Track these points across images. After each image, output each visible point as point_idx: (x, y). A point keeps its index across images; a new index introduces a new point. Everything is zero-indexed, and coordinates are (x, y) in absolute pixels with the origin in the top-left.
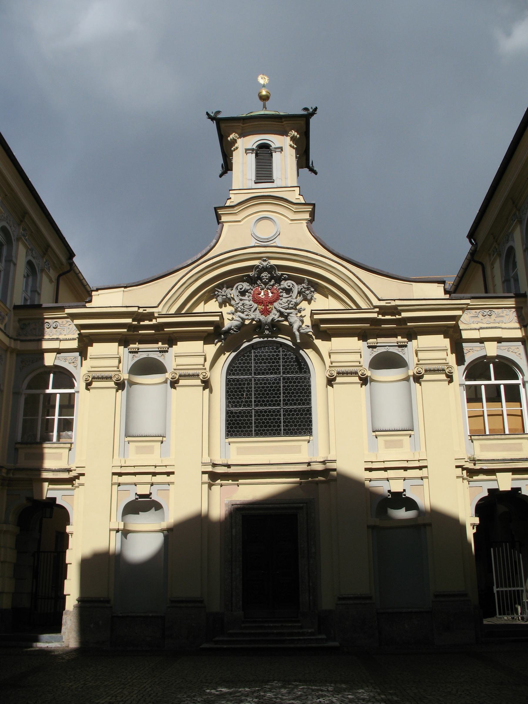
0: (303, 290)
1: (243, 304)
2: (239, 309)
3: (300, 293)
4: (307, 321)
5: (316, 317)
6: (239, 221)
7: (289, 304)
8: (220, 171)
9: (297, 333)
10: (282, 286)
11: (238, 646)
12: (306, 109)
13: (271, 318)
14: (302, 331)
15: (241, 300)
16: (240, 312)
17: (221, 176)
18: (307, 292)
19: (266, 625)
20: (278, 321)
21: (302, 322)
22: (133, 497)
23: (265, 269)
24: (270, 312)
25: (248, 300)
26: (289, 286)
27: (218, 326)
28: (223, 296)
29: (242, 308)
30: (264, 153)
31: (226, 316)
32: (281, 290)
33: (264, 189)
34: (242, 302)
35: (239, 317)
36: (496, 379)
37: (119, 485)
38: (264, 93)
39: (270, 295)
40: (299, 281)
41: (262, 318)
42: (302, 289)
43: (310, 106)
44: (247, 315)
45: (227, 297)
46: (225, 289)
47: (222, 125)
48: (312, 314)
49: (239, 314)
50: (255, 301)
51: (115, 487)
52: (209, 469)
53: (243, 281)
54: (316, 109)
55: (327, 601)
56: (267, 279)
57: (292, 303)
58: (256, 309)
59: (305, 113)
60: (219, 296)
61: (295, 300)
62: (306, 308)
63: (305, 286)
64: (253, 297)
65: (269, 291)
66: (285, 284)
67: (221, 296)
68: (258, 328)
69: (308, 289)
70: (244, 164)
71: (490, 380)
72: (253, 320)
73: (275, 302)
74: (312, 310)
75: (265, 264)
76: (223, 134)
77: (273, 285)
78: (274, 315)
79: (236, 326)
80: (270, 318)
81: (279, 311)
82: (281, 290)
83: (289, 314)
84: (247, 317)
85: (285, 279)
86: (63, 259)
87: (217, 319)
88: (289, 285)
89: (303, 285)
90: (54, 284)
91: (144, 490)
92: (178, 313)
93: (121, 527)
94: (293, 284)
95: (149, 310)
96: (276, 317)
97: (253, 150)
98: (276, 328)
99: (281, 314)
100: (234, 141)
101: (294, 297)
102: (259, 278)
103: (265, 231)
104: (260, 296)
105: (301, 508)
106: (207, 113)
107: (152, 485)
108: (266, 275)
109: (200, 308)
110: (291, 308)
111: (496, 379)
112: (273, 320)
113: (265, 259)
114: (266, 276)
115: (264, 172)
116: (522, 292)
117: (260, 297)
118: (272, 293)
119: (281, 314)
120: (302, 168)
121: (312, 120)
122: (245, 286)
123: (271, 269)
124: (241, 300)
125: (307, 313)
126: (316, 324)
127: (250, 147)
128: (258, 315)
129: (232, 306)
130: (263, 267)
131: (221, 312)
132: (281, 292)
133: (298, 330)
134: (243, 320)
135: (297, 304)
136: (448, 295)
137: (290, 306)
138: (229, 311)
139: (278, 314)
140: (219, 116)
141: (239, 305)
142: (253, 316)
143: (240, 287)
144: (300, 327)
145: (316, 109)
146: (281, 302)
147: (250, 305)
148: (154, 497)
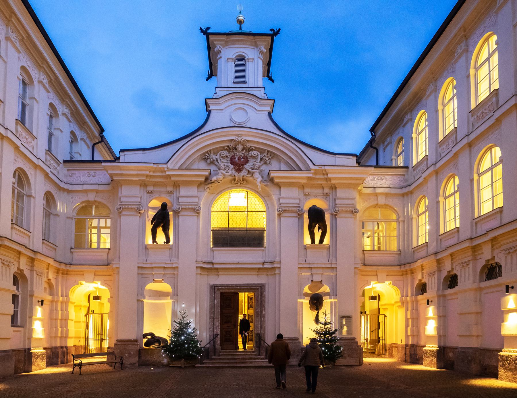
6: (222, 110)
8: (207, 76)
10: (250, 155)
11: (217, 365)
12: (272, 30)
17: (207, 80)
30: (241, 62)
38: (241, 18)
39: (242, 160)
43: (276, 29)
47: (211, 38)
54: (280, 29)
70: (226, 71)
76: (211, 46)
86: (97, 134)
90: (91, 149)
97: (233, 59)
100: (219, 52)
103: (239, 118)
106: (201, 28)
109: (195, 166)
115: (240, 76)
119: (249, 172)
121: (275, 38)
127: (230, 57)
136: (376, 192)
139: (247, 172)
140: (209, 31)
143: (223, 154)
145: (280, 29)
146: (249, 164)
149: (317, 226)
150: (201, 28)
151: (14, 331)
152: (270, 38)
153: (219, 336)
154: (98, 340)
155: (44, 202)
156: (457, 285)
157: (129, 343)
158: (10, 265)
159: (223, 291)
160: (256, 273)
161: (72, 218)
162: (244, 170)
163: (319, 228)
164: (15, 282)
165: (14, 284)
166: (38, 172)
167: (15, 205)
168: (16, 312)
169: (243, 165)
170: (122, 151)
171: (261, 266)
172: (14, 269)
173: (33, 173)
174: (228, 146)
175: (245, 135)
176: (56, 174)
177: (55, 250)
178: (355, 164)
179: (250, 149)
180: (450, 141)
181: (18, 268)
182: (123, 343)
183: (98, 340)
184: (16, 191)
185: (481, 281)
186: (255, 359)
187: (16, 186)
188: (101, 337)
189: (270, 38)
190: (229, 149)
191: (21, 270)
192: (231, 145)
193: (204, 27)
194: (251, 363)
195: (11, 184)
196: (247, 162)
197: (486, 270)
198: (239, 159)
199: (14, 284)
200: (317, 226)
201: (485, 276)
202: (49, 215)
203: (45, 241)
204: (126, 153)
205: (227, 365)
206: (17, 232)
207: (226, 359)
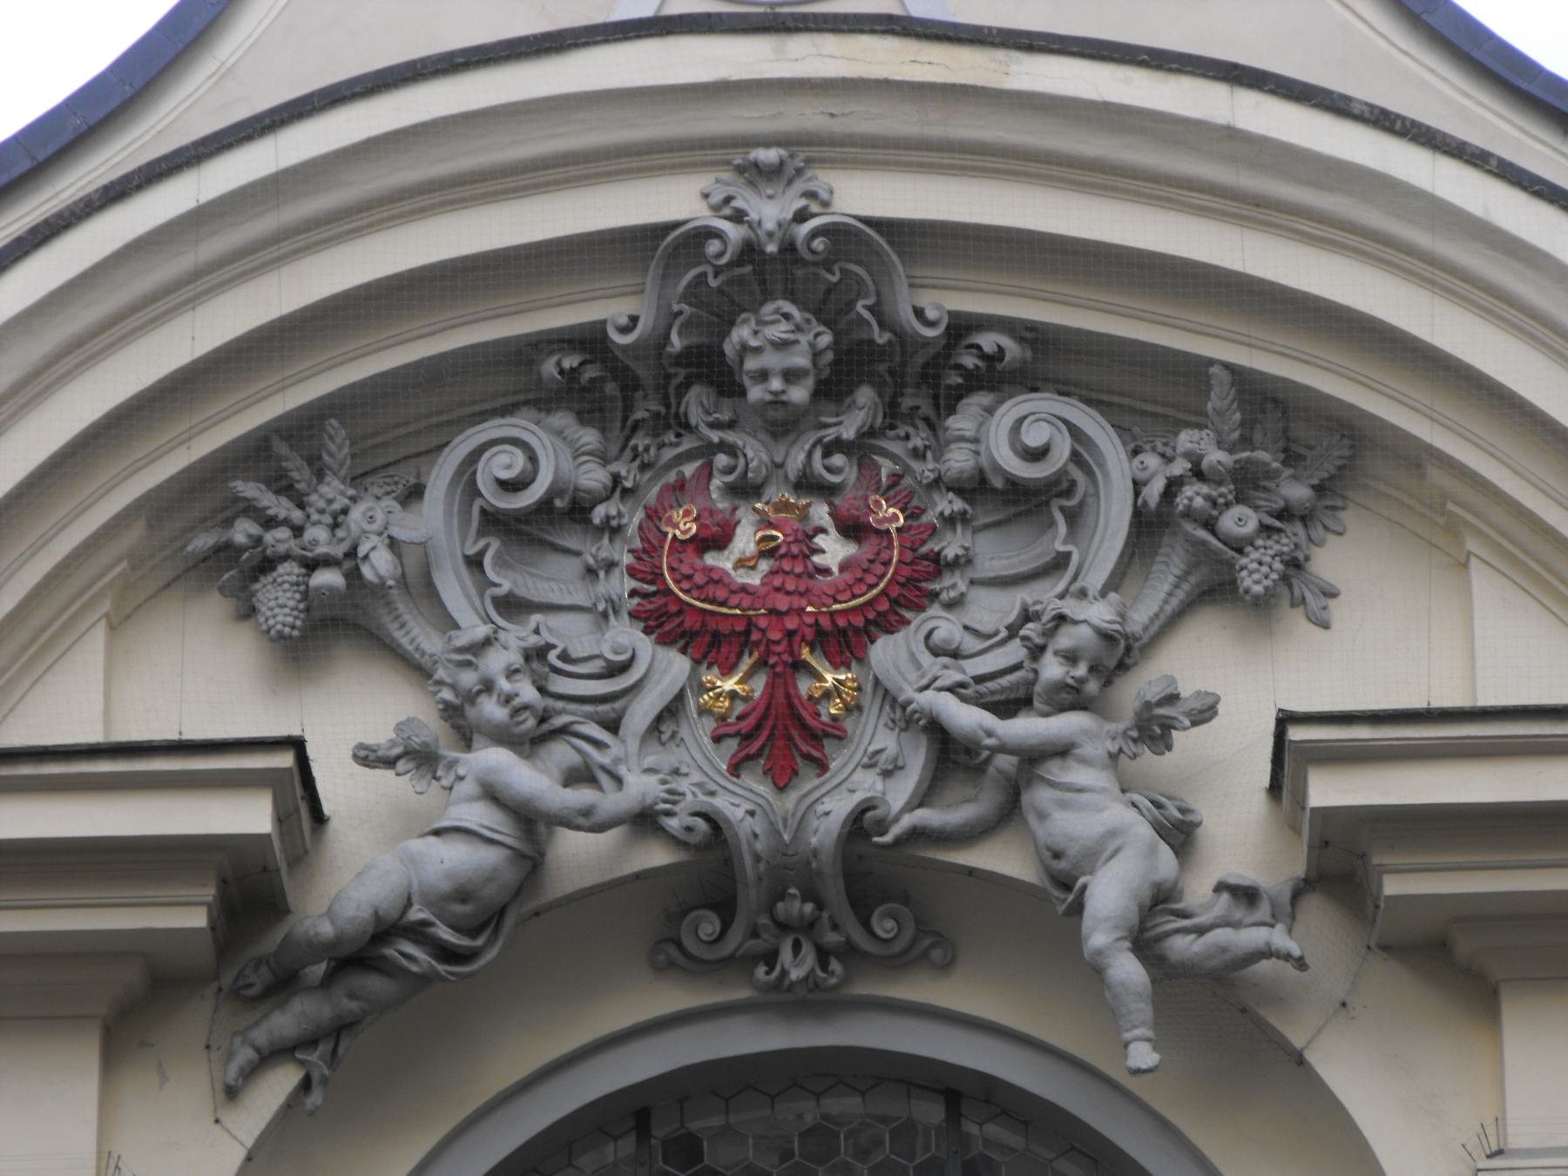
0: (1193, 495)
1: (536, 654)
2: (492, 710)
3: (1149, 526)
4: (1241, 836)
5: (1329, 790)
7: (1037, 652)
9: (1127, 970)
10: (959, 460)
13: (839, 807)
14: (1182, 946)
15: (512, 606)
16: (503, 737)
18: (1239, 520)
20: (918, 834)
21: (1180, 834)
23: (767, 270)
24: (836, 733)
25: (585, 615)
26: (1037, 455)
27: (250, 887)
28: (311, 565)
29: (527, 692)
31: (337, 781)
32: (948, 504)
34: (518, 635)
35: (492, 794)
40: (1142, 422)
41: (743, 803)
42: (1172, 487)
44: (580, 776)
45: (354, 576)
46: (333, 490)
48: (1287, 763)
49: (494, 759)
50: (663, 620)
53: (544, 401)
56: (791, 376)
57: (1066, 639)
58: (672, 710)
60: (267, 565)
61: (1100, 613)
62: (1239, 686)
63: (1215, 457)
64: (644, 570)
65: (820, 513)
66: (1005, 433)
67: (289, 571)
68: (705, 901)
69: (1246, 484)
72: (645, 821)
73: (885, 620)
74: (1286, 720)
75: (770, 211)
77: (860, 449)
78: (874, 777)
79: (462, 894)
80: (830, 803)
81: (909, 720)
82: (948, 504)
83: (1034, 758)
84: (581, 796)
85: (996, 378)
87: (250, 816)
88: (1034, 436)
89: (1186, 439)
94: (1075, 432)
96: (899, 793)
98: (881, 896)
99: (951, 756)
101: (1096, 578)
102: (715, 370)
104: (722, 561)
108: (780, 331)
110: (1070, 698)
112: (861, 824)
113: (769, 155)
114: (782, 345)
117: (716, 579)
118: (852, 529)
120: (1126, 1057)
122: (551, 452)
123: (833, 270)
124: (512, 606)
125: (1225, 771)
126: (1340, 860)
128: (702, 779)
129: (418, 670)
130: (750, 251)
131: (296, 745)
132: (950, 521)
133: (1144, 943)
134: (531, 822)
135: (1119, 654)
137: (1052, 669)
138: (380, 734)
139: (917, 761)
141: (496, 662)
142: (640, 786)
143: (506, 463)
144: (1161, 901)
146: (947, 627)
147: (615, 670)
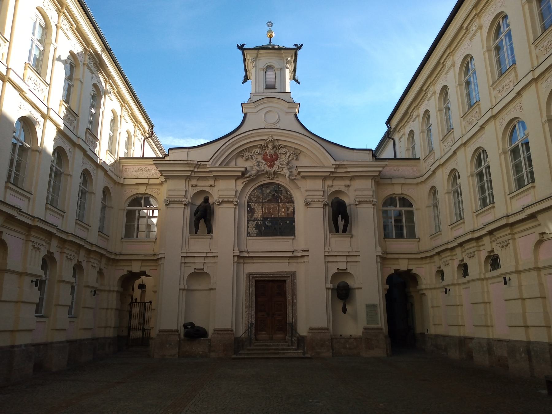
12: (296, 45)
17: (243, 83)
19: (269, 344)
22: (193, 271)
33: (270, 93)
36: (400, 207)
37: (185, 263)
39: (273, 156)
43: (299, 43)
50: (264, 160)
51: (183, 265)
52: (238, 254)
54: (302, 45)
55: (302, 330)
59: (296, 47)
71: (405, 211)
91: (200, 266)
92: (220, 165)
93: (186, 288)
95: (203, 163)
105: (289, 277)
106: (237, 45)
107: (204, 263)
111: (400, 207)
116: (417, 157)
121: (300, 52)
145: (302, 45)
148: (205, 270)
149: (340, 216)
150: (237, 45)
151: (38, 322)
152: (294, 51)
153: (254, 326)
154: (140, 330)
155: (81, 180)
156: (498, 268)
157: (170, 333)
158: (40, 248)
159: (258, 279)
160: (287, 261)
161: (124, 210)
162: (275, 166)
163: (342, 219)
164: (44, 266)
165: (42, 269)
166: (77, 151)
167: (52, 183)
168: (41, 300)
169: (274, 161)
170: (170, 149)
171: (291, 254)
172: (44, 253)
173: (95, 172)
174: (261, 145)
175: (276, 135)
176: (72, 128)
177: (63, 216)
178: (371, 158)
179: (279, 147)
180: (450, 139)
181: (48, 252)
182: (165, 333)
183: (140, 330)
184: (54, 169)
185: (486, 271)
186: (287, 349)
187: (54, 164)
188: (143, 326)
189: (294, 51)
190: (261, 147)
191: (52, 253)
192: (263, 143)
193: (240, 44)
194: (284, 353)
195: (50, 163)
196: (277, 158)
197: (490, 261)
198: (271, 155)
199: (42, 269)
200: (340, 216)
201: (489, 267)
202: (105, 207)
203: (78, 222)
204: (173, 151)
205: (261, 356)
206: (12, 193)
207: (260, 349)
